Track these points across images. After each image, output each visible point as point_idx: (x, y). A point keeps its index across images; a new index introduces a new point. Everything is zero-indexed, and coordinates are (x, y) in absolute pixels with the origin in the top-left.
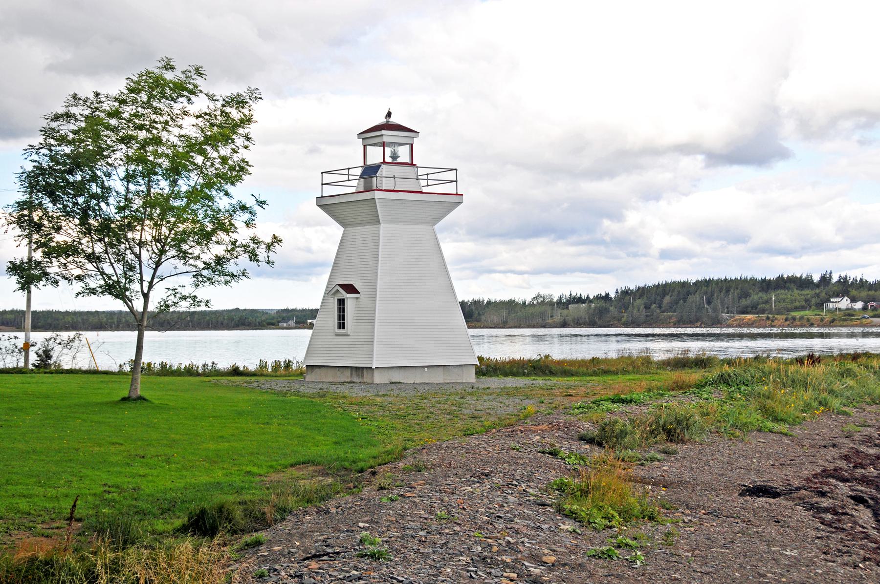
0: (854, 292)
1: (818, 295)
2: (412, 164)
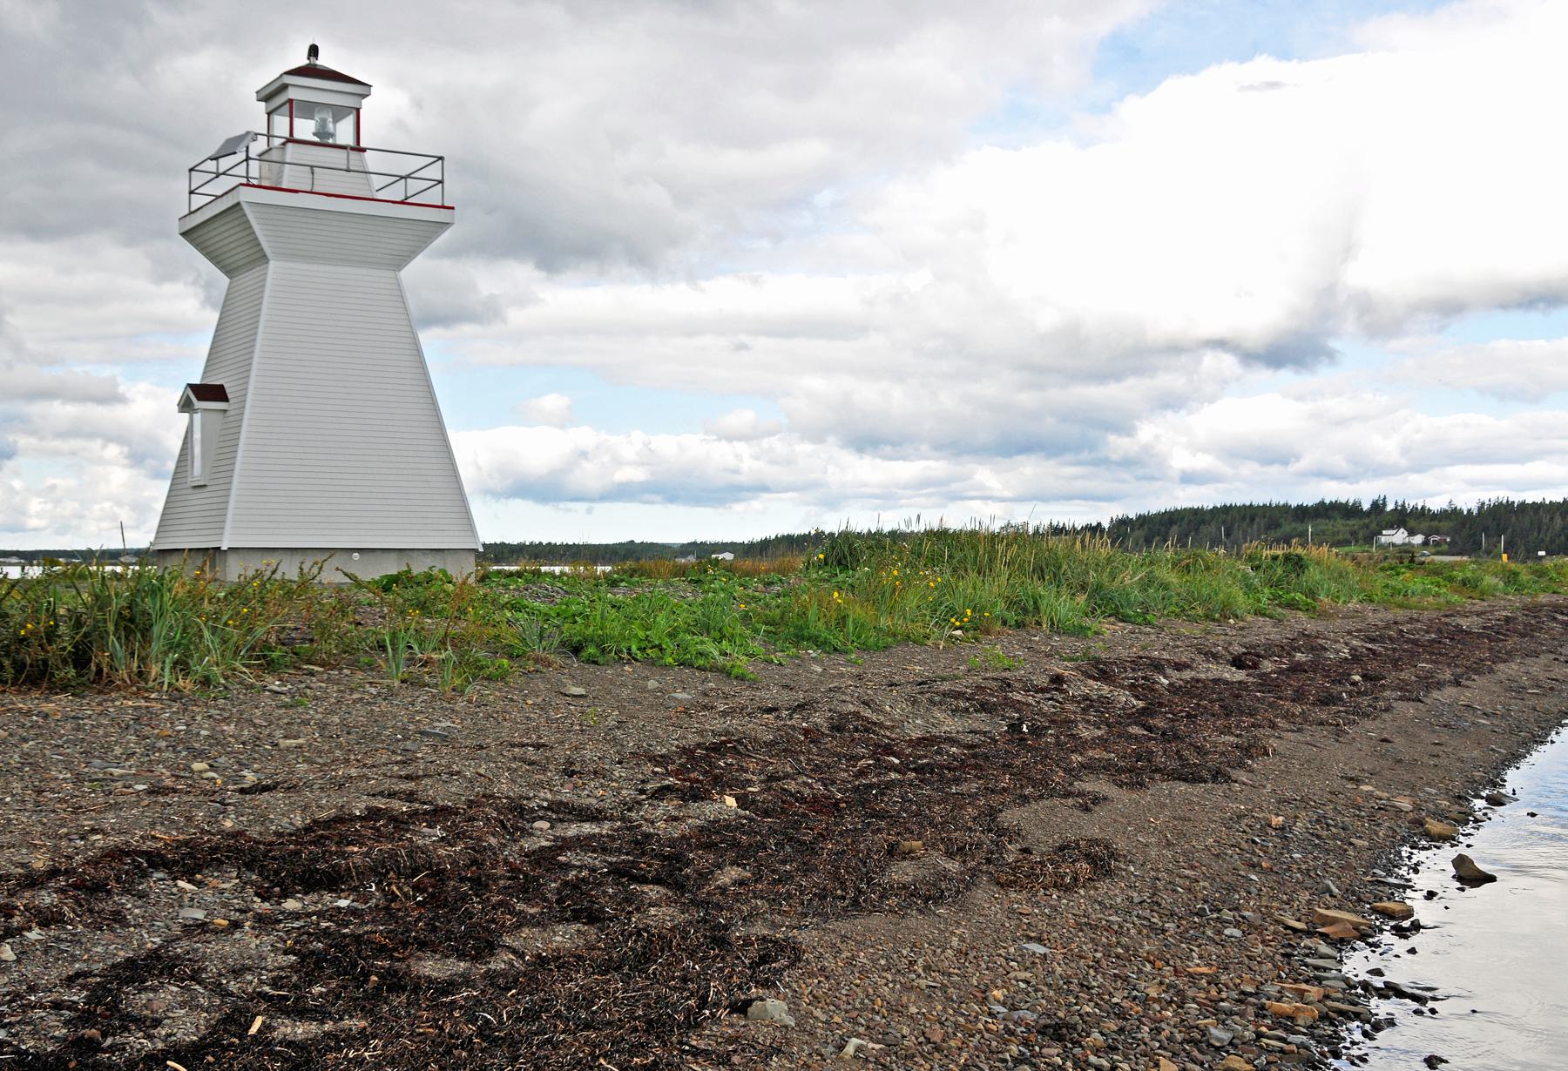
0: (1412, 523)
1: (1367, 526)
2: (359, 149)
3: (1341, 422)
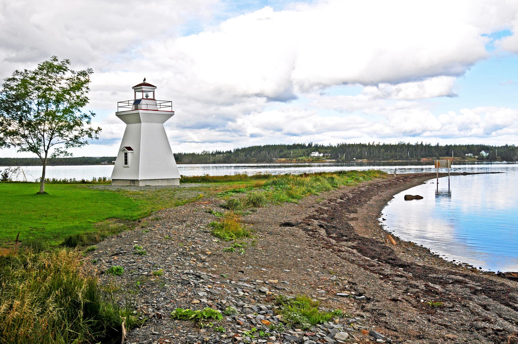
0: (320, 150)
1: (307, 151)
3: (295, 119)
